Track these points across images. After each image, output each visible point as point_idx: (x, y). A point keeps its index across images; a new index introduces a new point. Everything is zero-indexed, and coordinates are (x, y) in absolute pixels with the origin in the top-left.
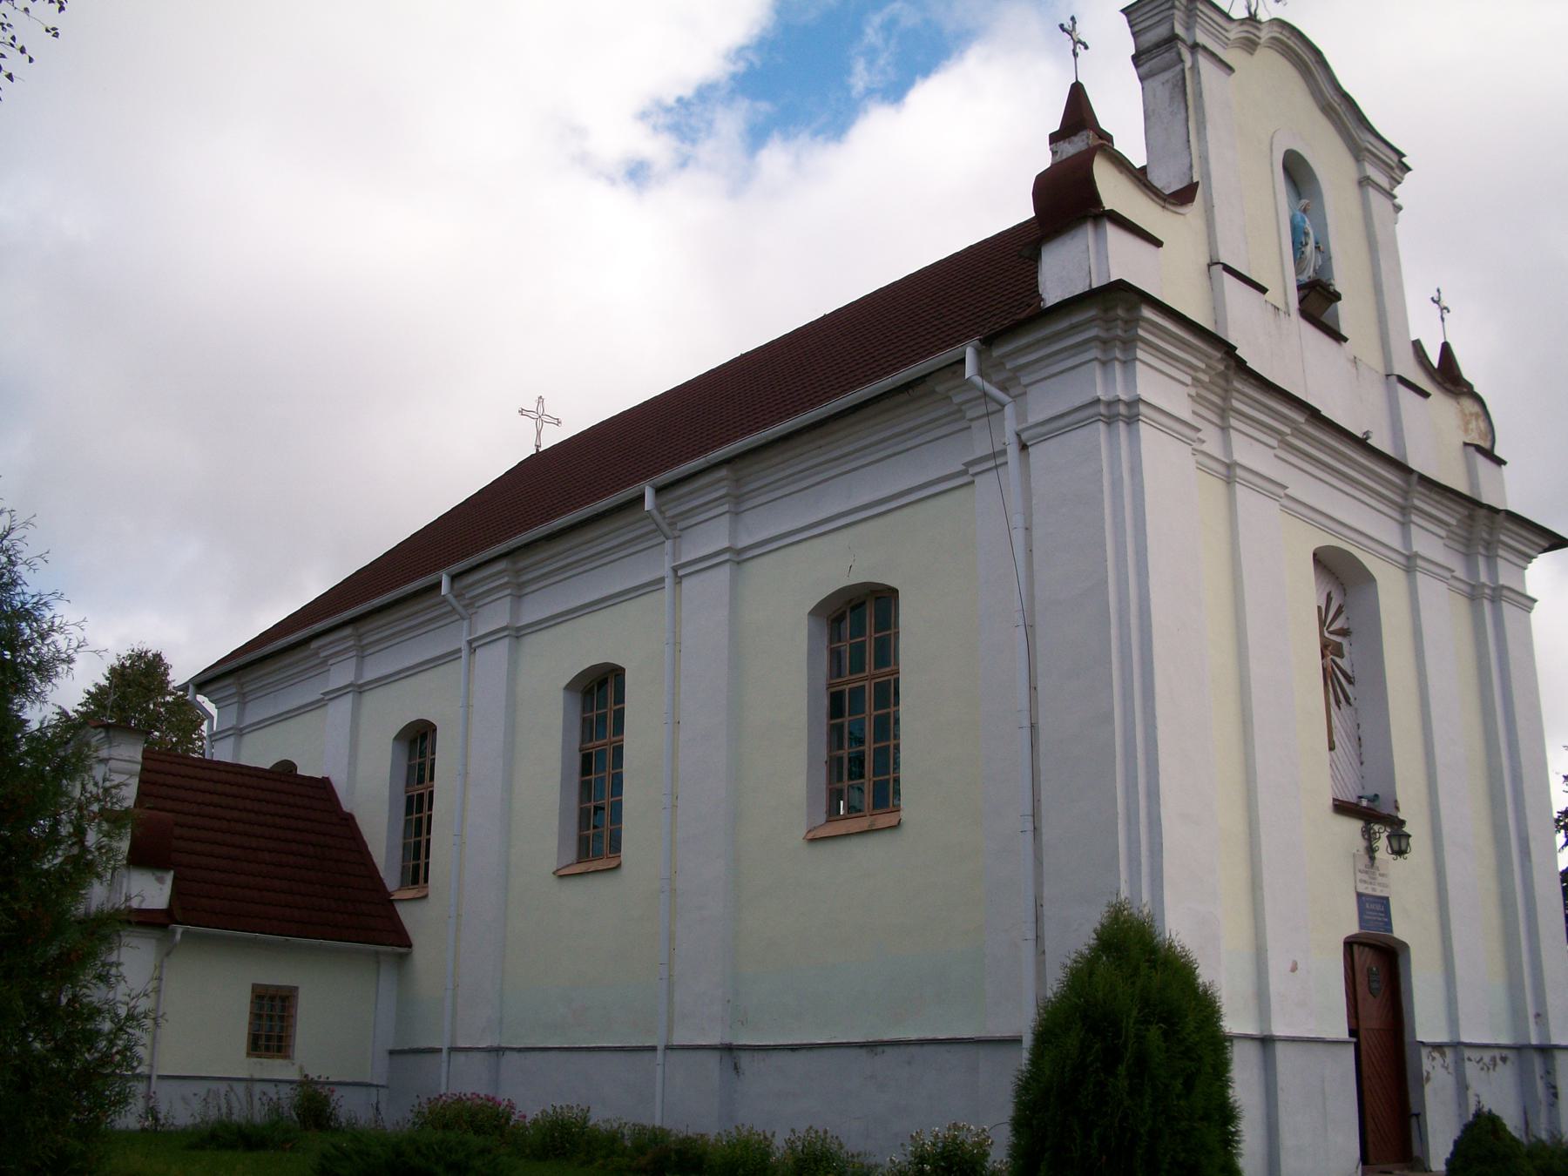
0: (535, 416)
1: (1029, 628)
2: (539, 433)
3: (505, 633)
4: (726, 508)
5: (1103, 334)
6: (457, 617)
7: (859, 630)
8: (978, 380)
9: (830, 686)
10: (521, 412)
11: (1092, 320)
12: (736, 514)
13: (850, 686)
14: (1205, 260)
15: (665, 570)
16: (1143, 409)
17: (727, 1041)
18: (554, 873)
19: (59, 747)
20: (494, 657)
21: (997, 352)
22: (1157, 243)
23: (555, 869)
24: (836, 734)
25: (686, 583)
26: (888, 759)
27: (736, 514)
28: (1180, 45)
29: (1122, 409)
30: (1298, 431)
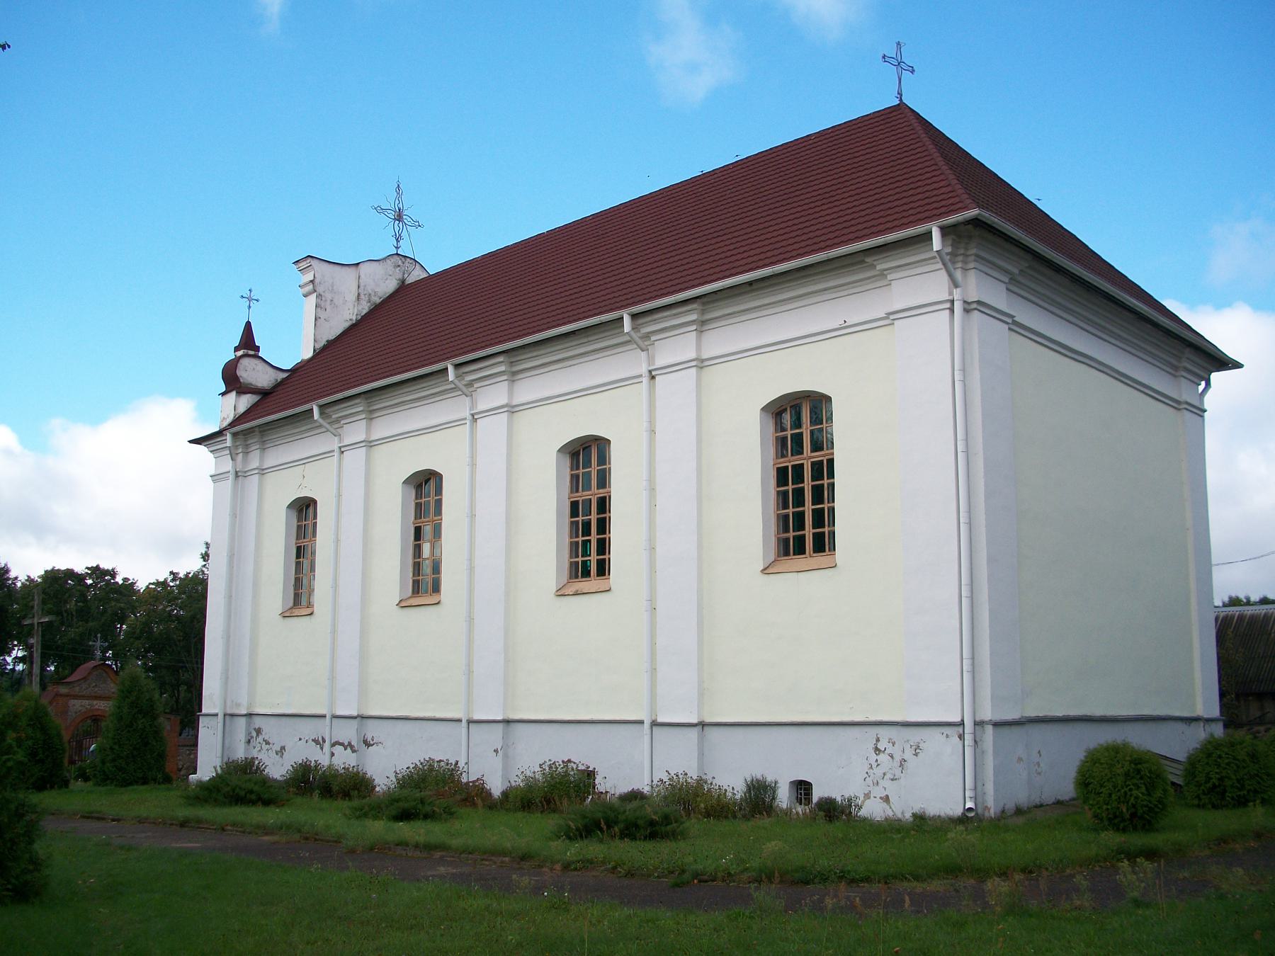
3: (506, 409)
6: (460, 393)
7: (588, 464)
8: (321, 421)
12: (700, 332)
13: (583, 498)
17: (506, 718)
18: (397, 605)
20: (355, 458)
22: (190, 442)
23: (762, 568)
24: (783, 499)
26: (824, 518)
27: (700, 332)
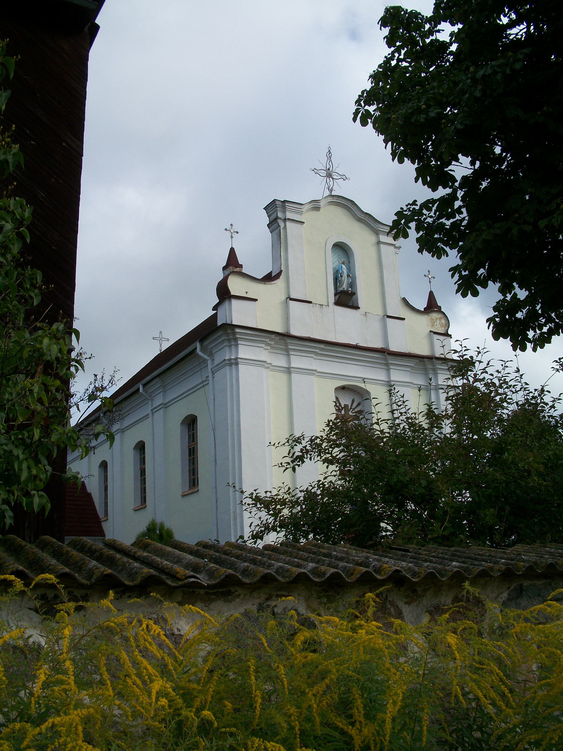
0: (163, 339)
1: (214, 430)
2: (161, 345)
4: (161, 390)
5: (226, 338)
9: (189, 446)
10: (154, 338)
11: (222, 334)
14: (284, 297)
15: (149, 411)
16: (239, 360)
19: (31, 471)
21: (205, 344)
25: (156, 414)
28: (279, 221)
29: (233, 361)
30: (322, 349)
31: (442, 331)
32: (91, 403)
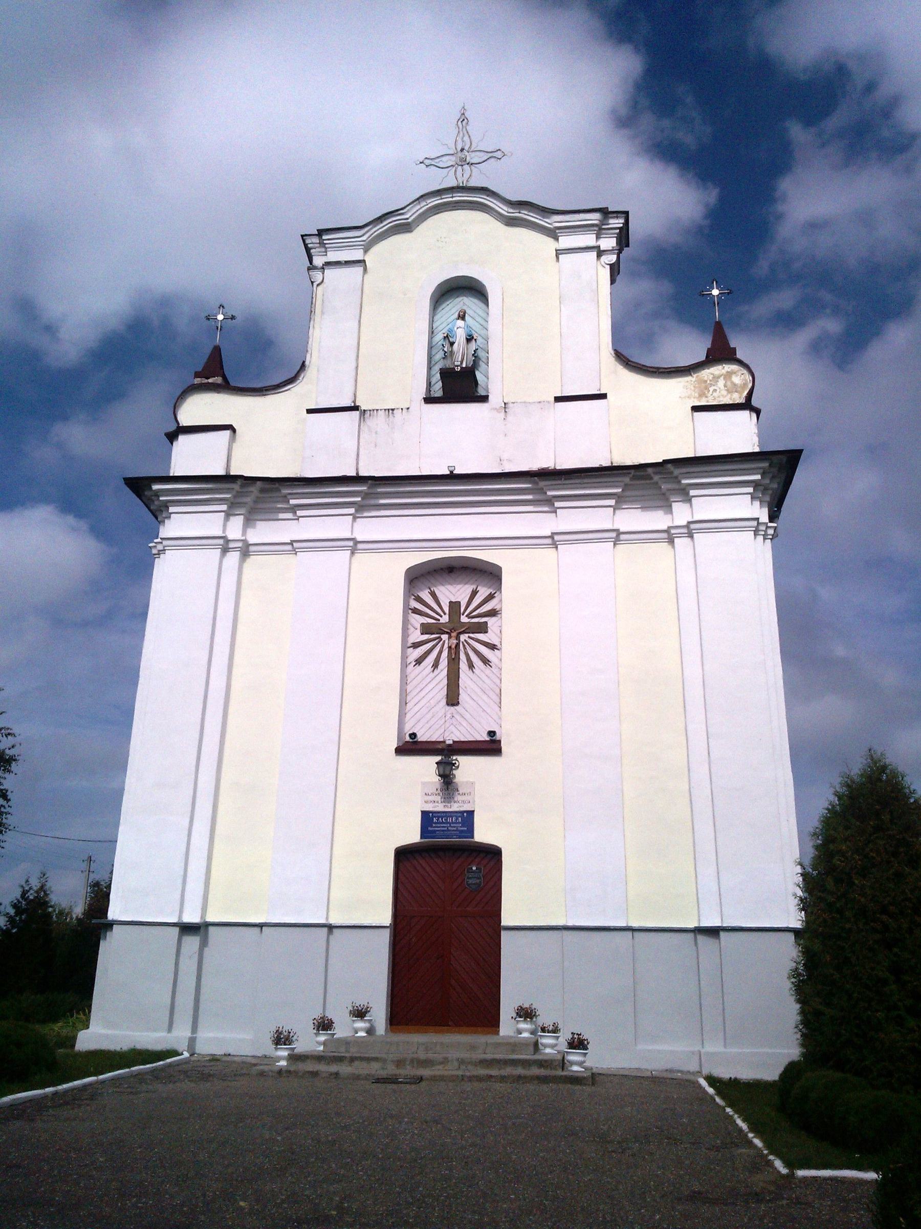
31: (739, 398)
32: (426, 637)
